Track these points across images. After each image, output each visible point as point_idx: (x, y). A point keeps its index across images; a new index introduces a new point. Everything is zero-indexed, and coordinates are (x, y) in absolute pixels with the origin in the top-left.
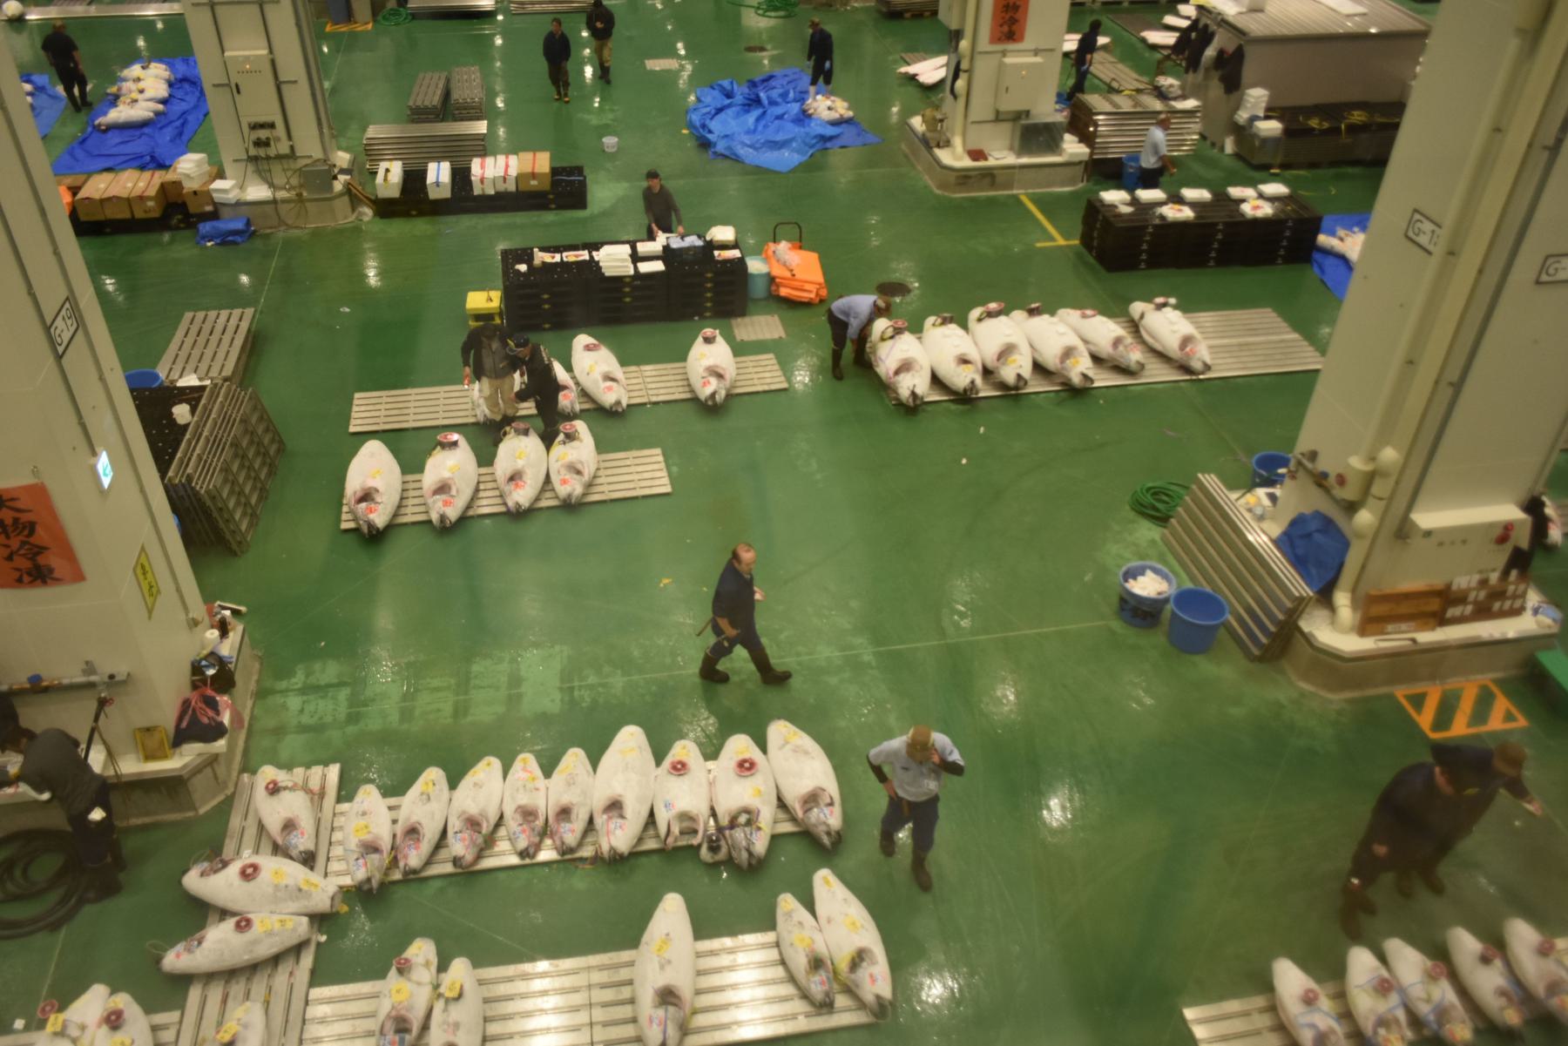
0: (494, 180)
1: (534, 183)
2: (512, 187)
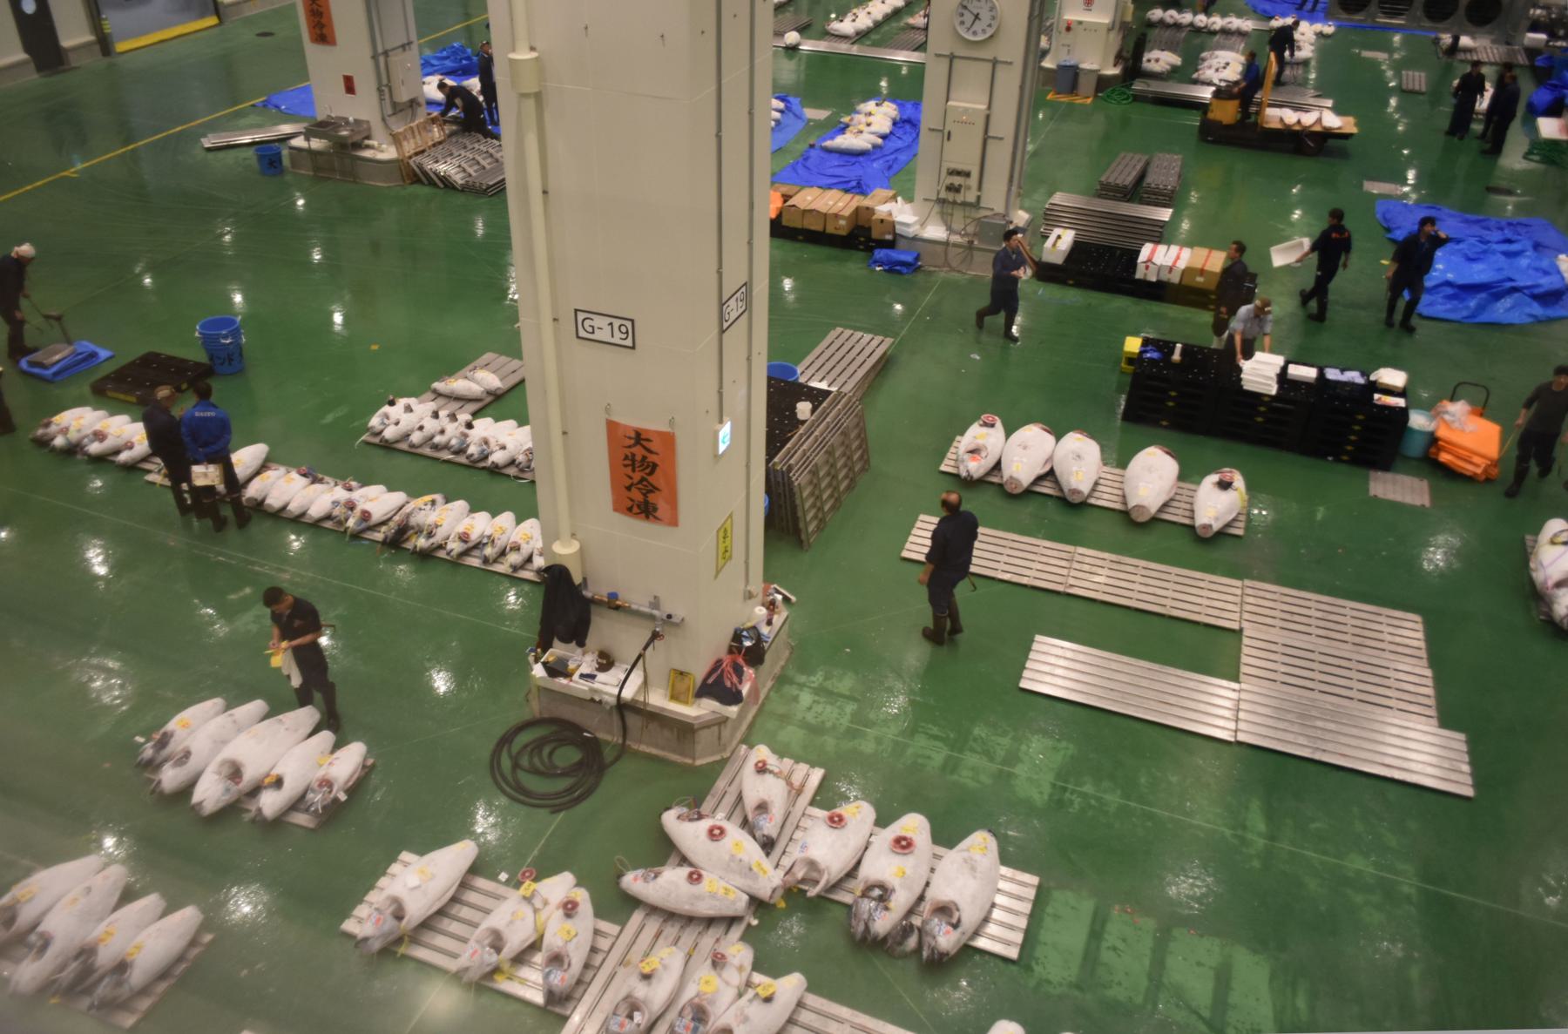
0: (1160, 268)
1: (1200, 279)
2: (1175, 278)
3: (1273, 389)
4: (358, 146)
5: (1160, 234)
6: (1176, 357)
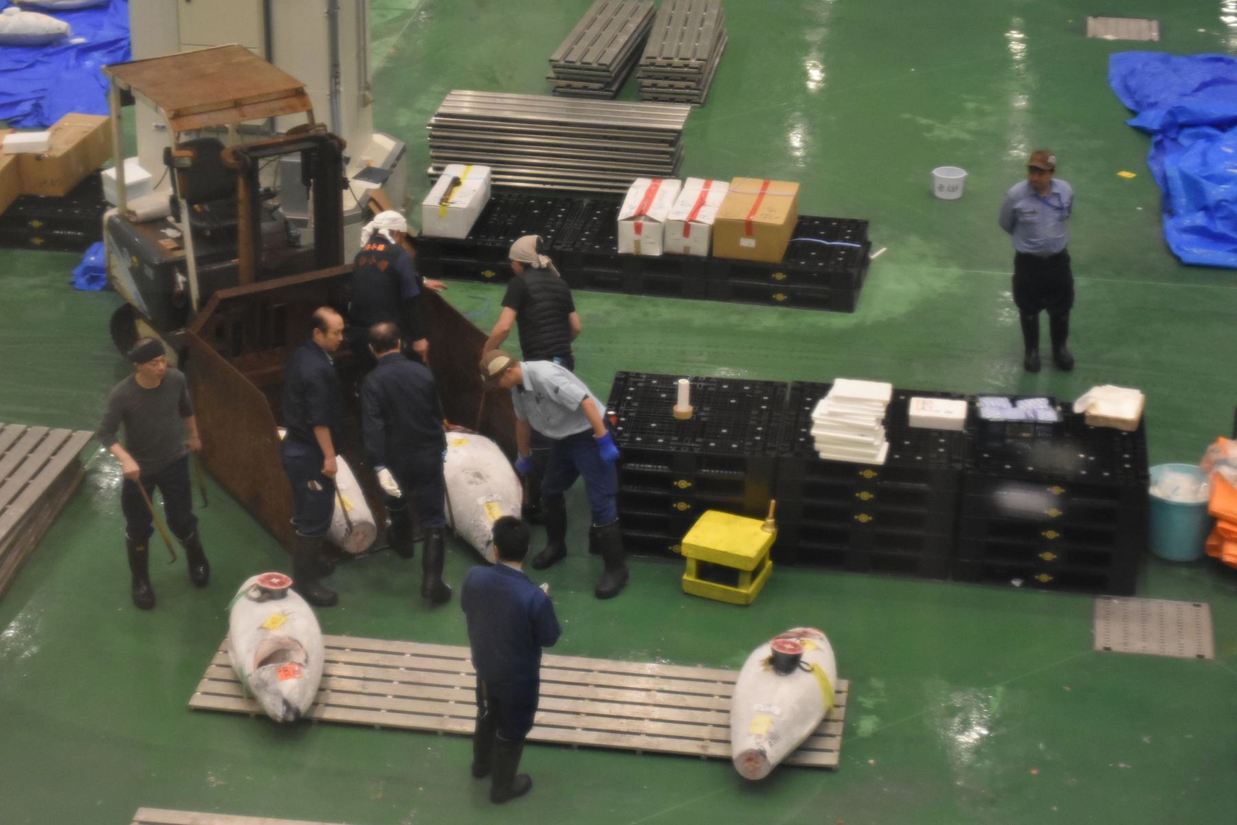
0: (664, 229)
1: (747, 243)
2: (699, 247)
3: (879, 453)
4: (171, 309)
5: (665, 157)
6: (683, 407)
